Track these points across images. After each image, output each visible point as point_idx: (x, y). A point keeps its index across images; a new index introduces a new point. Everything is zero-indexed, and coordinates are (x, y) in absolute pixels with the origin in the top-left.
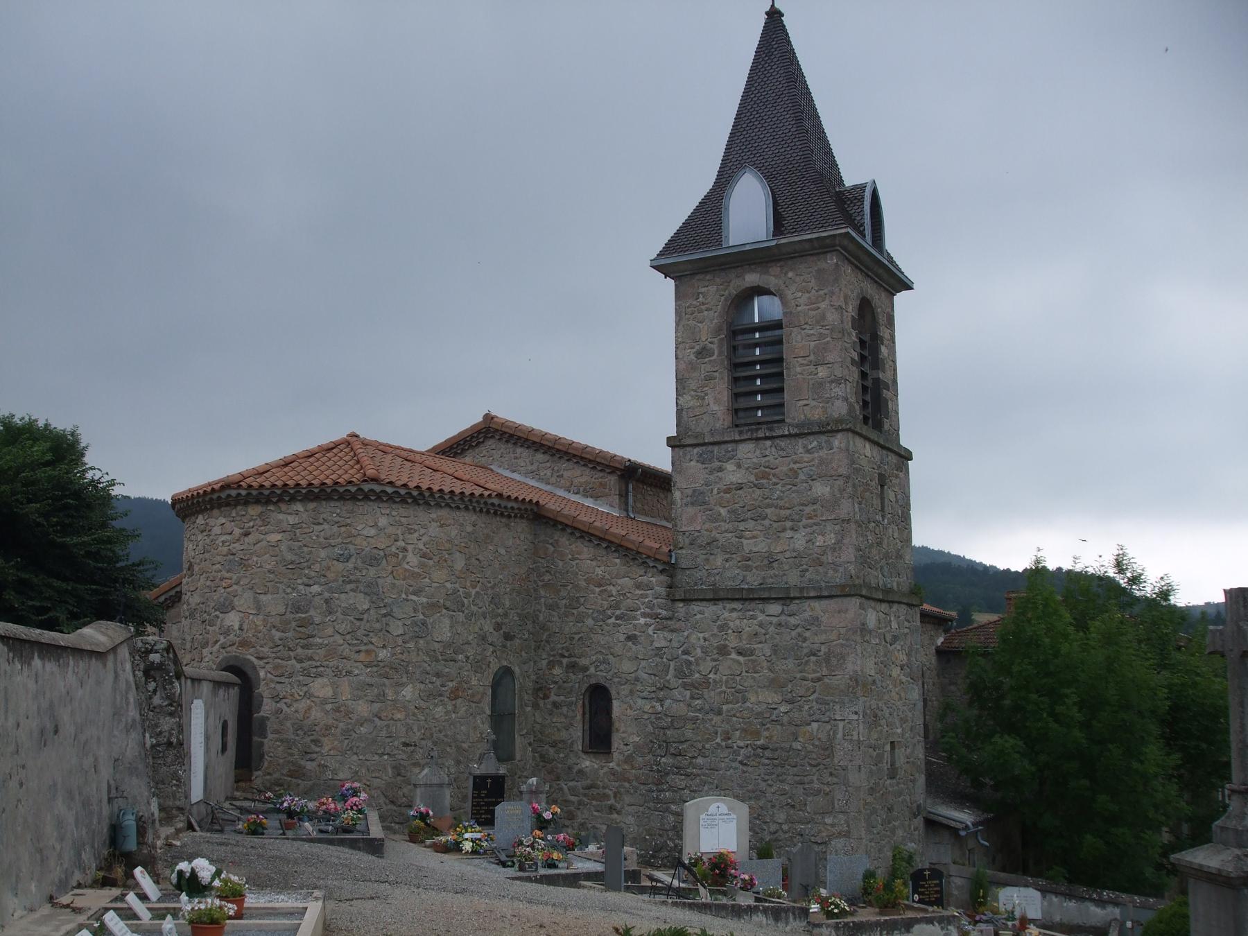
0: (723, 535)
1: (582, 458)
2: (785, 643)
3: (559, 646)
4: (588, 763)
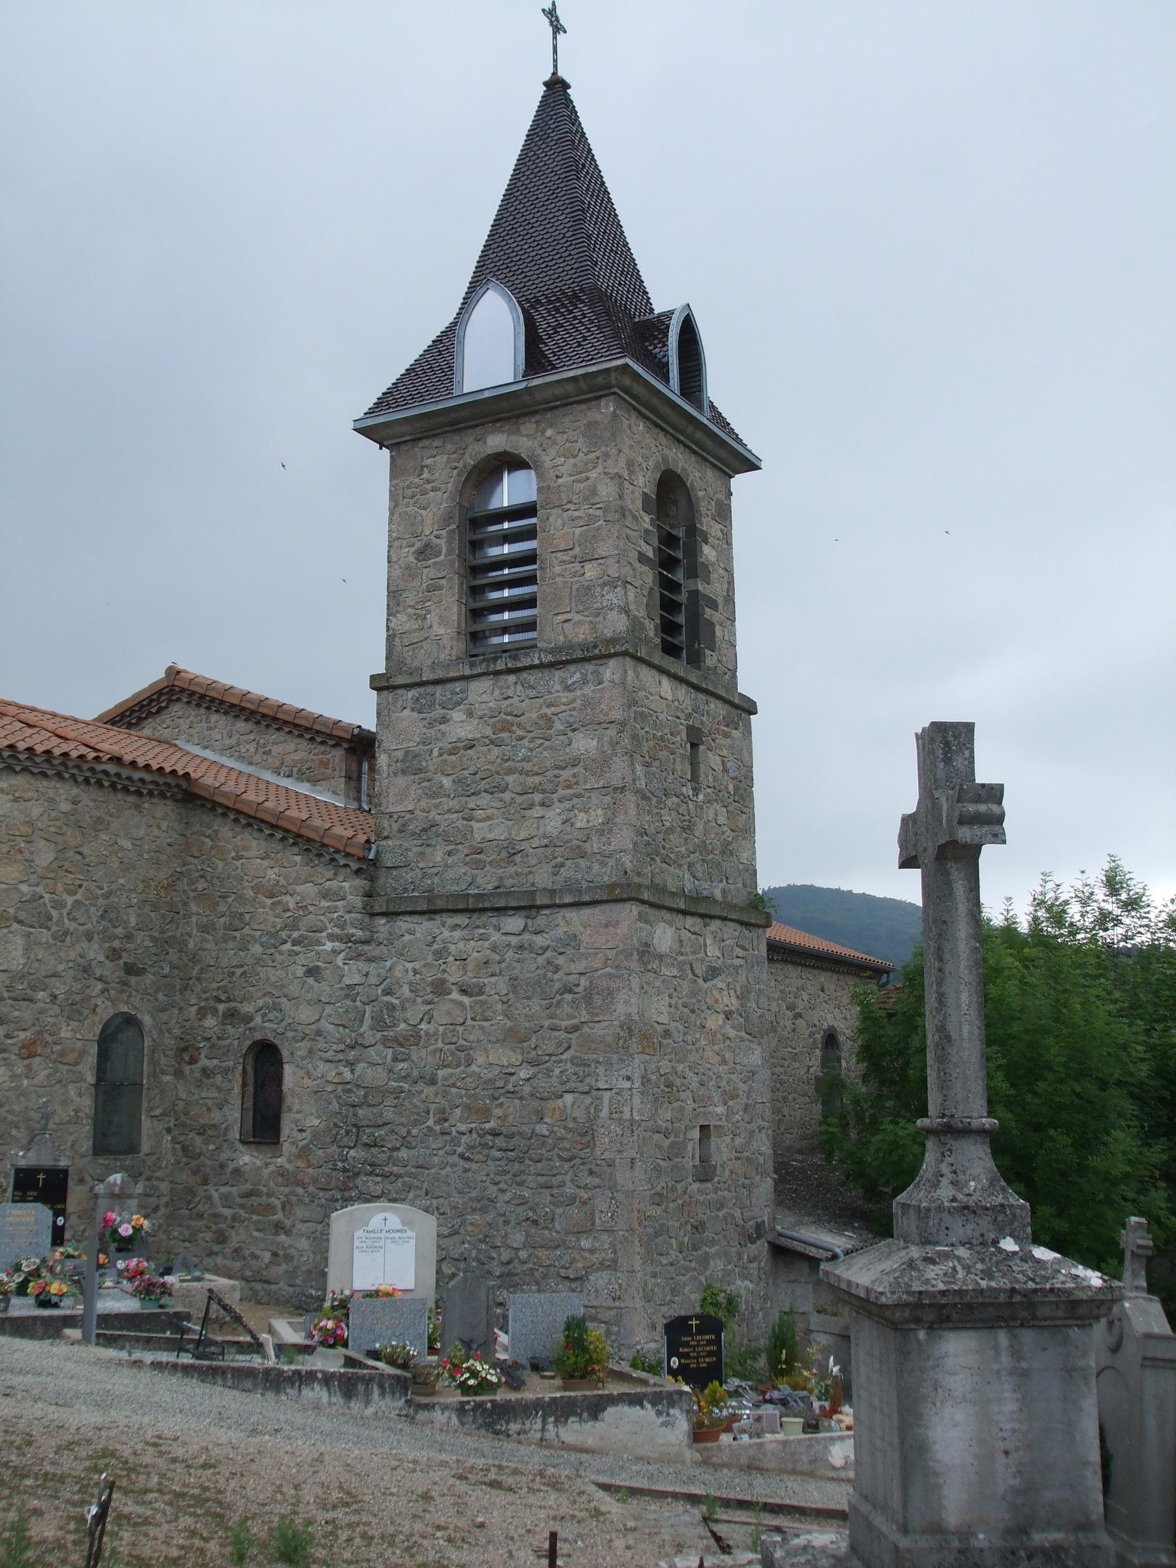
0: (446, 816)
1: (296, 726)
2: (528, 975)
3: (215, 985)
4: (247, 1159)
